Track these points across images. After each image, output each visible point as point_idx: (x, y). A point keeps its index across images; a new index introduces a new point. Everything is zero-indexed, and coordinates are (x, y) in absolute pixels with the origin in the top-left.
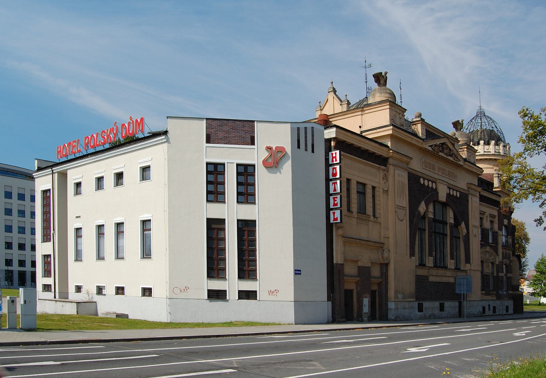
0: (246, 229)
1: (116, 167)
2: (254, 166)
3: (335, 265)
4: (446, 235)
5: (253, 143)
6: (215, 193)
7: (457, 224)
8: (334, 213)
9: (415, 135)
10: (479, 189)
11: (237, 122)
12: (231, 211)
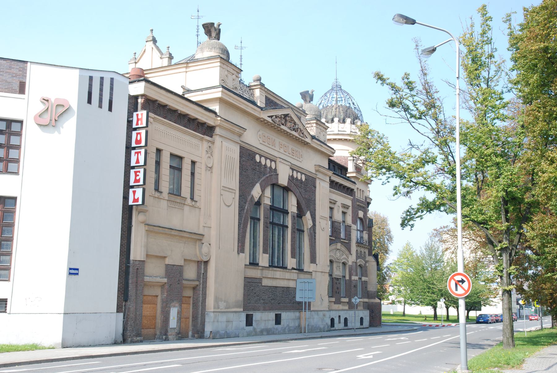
3: (131, 262)
4: (287, 227)
8: (134, 192)
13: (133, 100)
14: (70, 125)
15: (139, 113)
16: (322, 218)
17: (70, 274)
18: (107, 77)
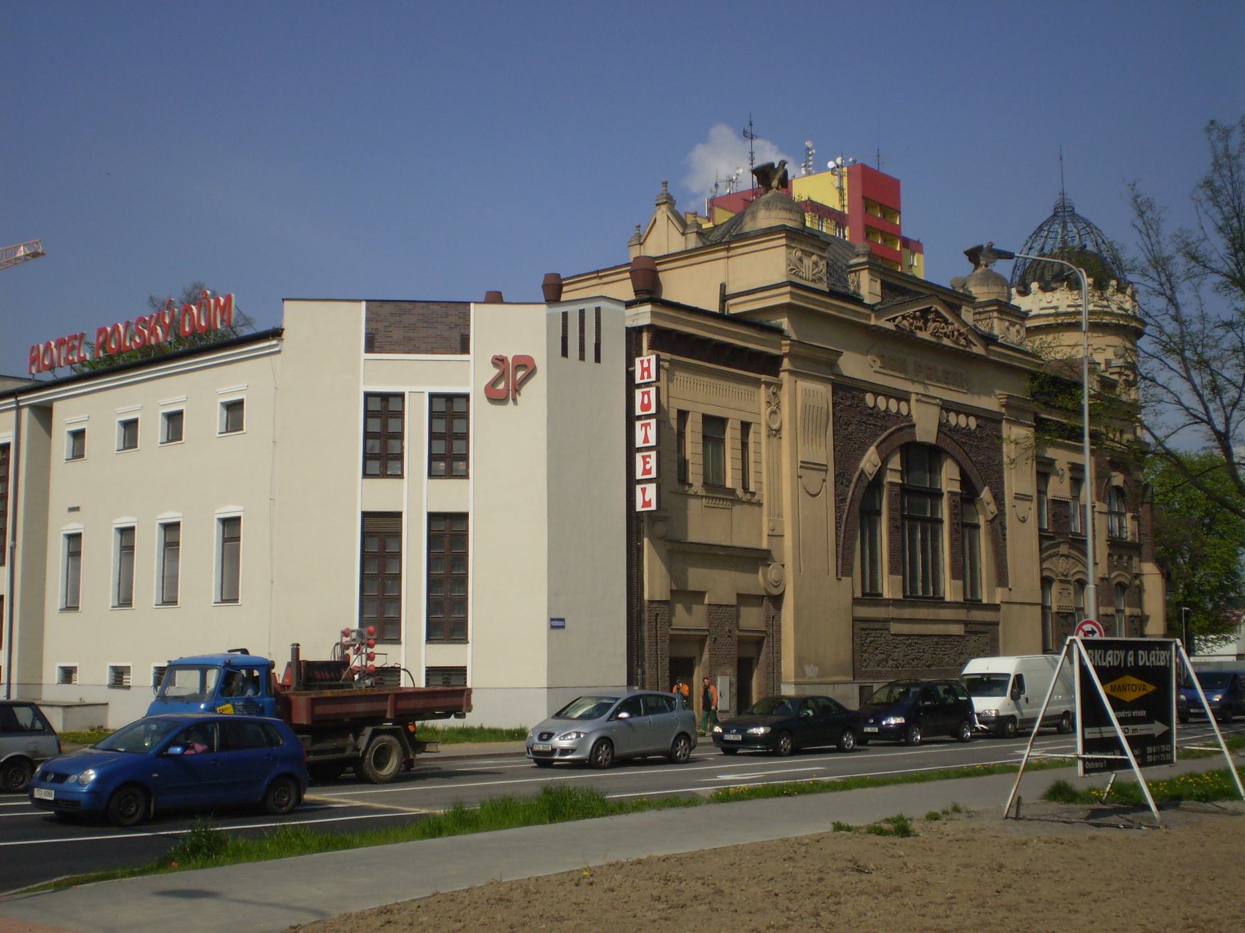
0: (448, 533)
1: (169, 400)
2: (466, 397)
3: (646, 604)
4: (941, 521)
5: (465, 349)
6: (382, 456)
7: (968, 495)
8: (644, 490)
9: (856, 299)
10: (1034, 406)
11: (432, 307)
12: (415, 495)
13: (633, 335)
14: (535, 392)
15: (645, 358)
16: (1020, 497)
17: (552, 627)
18: (590, 308)
